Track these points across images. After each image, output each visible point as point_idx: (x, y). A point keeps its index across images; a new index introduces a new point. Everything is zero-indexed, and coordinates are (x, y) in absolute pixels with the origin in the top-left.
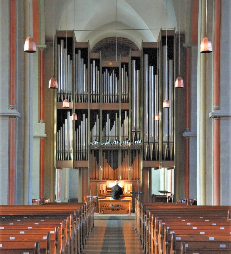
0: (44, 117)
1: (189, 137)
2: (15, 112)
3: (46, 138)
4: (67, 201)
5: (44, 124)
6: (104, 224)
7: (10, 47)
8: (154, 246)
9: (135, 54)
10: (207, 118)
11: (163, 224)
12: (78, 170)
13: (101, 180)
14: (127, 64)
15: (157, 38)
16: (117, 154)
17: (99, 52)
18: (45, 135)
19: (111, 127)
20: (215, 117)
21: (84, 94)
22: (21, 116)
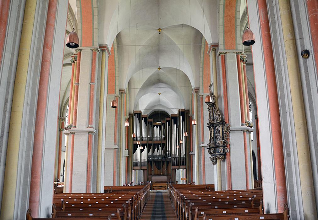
0: (128, 148)
1: (192, 155)
2: (116, 147)
3: (128, 156)
4: (137, 185)
5: (127, 150)
6: (154, 194)
7: (115, 119)
8: (178, 205)
9: (168, 119)
10: (199, 147)
11: (192, 204)
12: (143, 171)
13: (153, 175)
14: (164, 124)
15: (177, 113)
16: (160, 163)
17: (152, 119)
18: (128, 155)
19: (158, 151)
20: (202, 147)
21: (144, 137)
22: (96, 132)
